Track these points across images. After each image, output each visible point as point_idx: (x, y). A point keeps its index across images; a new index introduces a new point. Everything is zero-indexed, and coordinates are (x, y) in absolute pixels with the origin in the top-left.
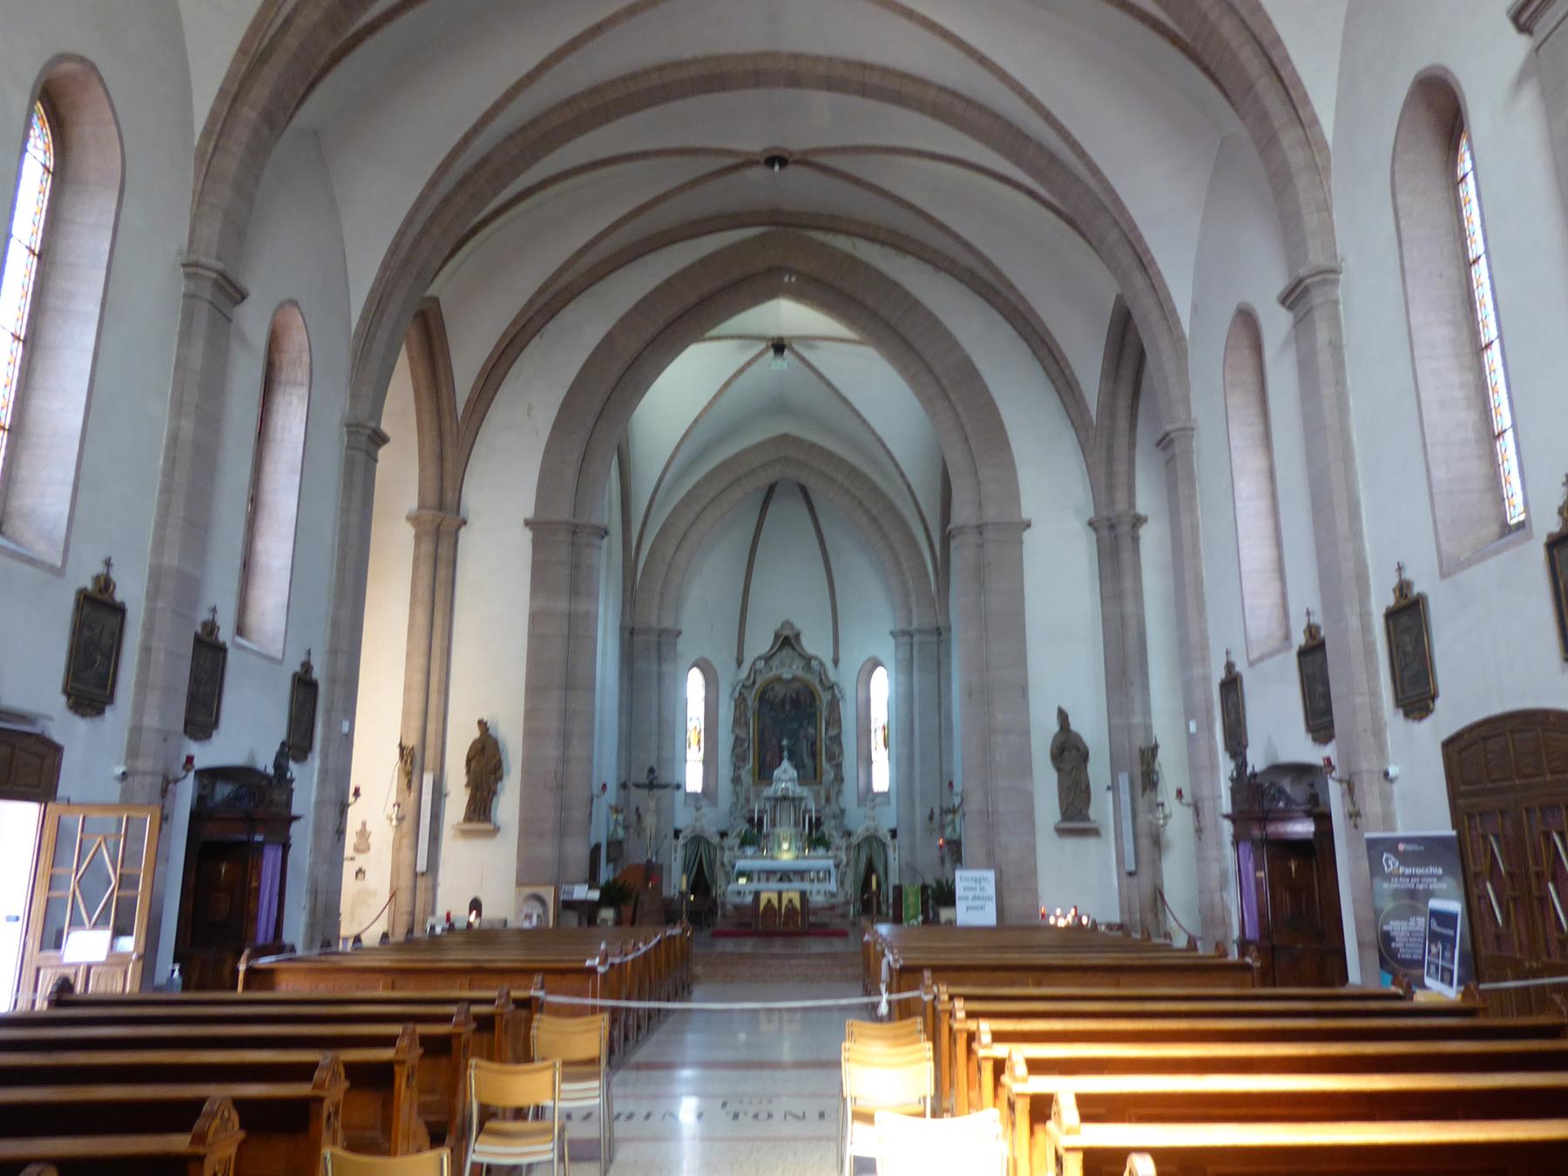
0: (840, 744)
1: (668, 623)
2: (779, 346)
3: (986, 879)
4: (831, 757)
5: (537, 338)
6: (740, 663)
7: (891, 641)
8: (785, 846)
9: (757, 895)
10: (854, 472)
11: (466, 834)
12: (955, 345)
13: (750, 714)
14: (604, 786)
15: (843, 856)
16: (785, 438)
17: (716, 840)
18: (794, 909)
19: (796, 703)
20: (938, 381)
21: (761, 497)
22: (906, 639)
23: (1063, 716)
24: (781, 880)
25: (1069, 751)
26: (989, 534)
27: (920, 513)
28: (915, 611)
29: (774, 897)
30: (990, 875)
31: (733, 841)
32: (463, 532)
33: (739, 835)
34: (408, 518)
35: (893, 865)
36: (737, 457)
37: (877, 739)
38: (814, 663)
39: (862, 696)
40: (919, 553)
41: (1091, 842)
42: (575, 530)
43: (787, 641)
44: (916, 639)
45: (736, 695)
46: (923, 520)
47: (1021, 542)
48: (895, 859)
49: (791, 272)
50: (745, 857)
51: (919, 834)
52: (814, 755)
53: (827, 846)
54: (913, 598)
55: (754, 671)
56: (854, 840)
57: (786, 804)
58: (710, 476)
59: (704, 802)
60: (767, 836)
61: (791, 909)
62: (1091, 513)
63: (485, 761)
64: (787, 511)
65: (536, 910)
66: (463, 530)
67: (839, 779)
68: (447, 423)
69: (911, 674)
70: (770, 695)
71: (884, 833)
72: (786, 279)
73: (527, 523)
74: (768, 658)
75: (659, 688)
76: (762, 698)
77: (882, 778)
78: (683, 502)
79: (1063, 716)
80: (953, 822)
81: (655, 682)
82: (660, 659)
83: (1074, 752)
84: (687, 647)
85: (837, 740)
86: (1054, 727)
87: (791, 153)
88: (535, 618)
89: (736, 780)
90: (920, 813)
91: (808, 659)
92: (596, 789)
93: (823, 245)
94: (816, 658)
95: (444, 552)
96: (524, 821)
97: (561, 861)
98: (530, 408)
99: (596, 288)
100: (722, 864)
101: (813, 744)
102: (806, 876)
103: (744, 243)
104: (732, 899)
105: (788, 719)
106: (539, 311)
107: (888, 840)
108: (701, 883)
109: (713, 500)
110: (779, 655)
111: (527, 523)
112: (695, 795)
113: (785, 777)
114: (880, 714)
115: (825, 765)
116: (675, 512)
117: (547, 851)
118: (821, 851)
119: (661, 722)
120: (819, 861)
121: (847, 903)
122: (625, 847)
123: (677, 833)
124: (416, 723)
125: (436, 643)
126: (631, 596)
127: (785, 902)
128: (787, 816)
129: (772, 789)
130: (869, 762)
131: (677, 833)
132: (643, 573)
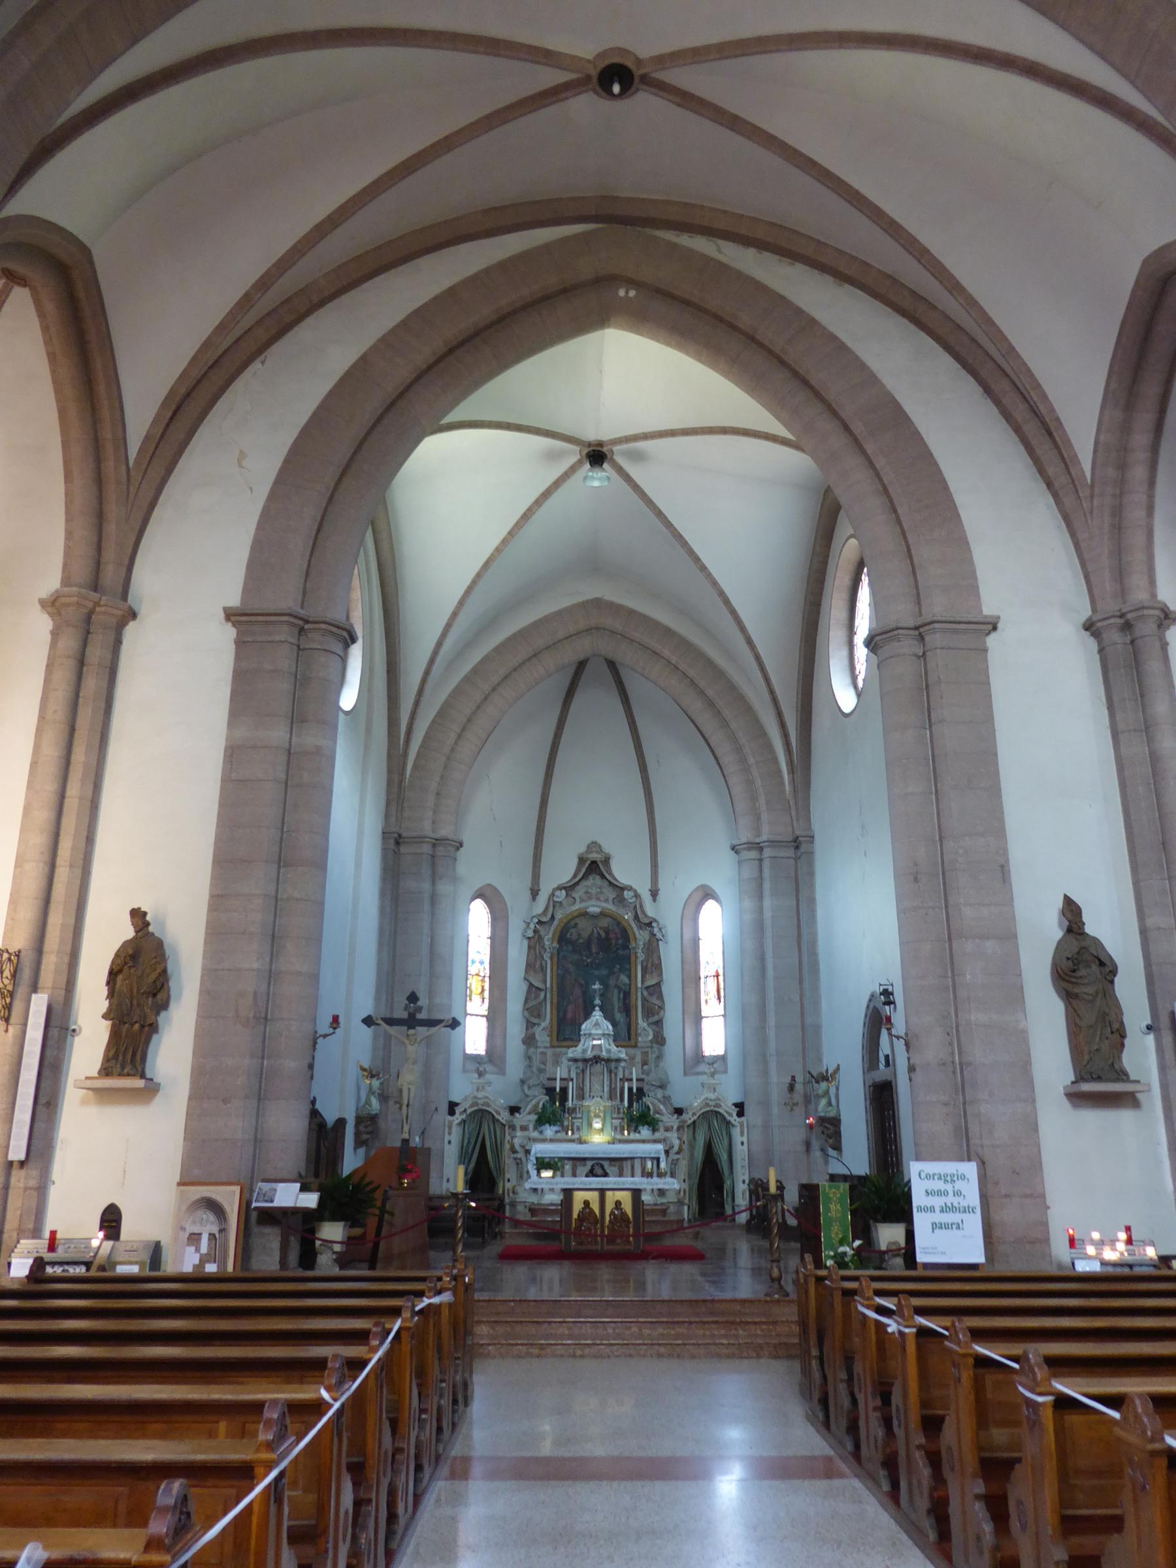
0: (660, 997)
1: (445, 831)
2: (597, 456)
3: (963, 1177)
4: (649, 1012)
5: (256, 365)
6: (535, 893)
7: (729, 858)
8: (597, 1125)
9: (568, 1193)
10: (684, 645)
11: (103, 1096)
12: (871, 379)
13: (547, 956)
14: (336, 1019)
15: (673, 1138)
16: (597, 604)
17: (504, 1117)
18: (624, 1214)
19: (605, 943)
20: (846, 427)
21: (571, 671)
22: (753, 854)
23: (1071, 912)
24: (592, 1173)
25: (1081, 967)
26: (935, 639)
27: (772, 692)
28: (765, 816)
29: (593, 1197)
30: (970, 1169)
31: (526, 1118)
32: (131, 630)
33: (533, 1111)
34: (43, 603)
36: (536, 625)
37: (708, 989)
39: (688, 935)
40: (769, 746)
41: (1124, 1117)
42: (302, 625)
43: (594, 867)
44: (767, 852)
45: (530, 934)
46: (775, 701)
47: (986, 650)
48: (742, 1142)
49: (631, 282)
50: (544, 1141)
51: (775, 1110)
52: (627, 1009)
53: (653, 1124)
54: (762, 801)
55: (552, 903)
56: (688, 1118)
57: (598, 1068)
58: (499, 650)
59: (489, 1067)
60: (573, 1110)
61: (619, 1217)
62: (1086, 612)
63: (141, 979)
64: (596, 701)
65: (207, 1226)
66: (131, 627)
68: (109, 465)
69: (761, 897)
70: (573, 934)
71: (727, 1108)
72: (622, 293)
73: (231, 615)
74: (569, 888)
75: (433, 914)
76: (562, 938)
77: (714, 1039)
78: (467, 679)
79: (1071, 912)
80: (827, 1093)
81: (427, 907)
82: (434, 878)
83: (1095, 967)
84: (472, 866)
85: (656, 990)
86: (1056, 933)
87: (639, 62)
88: (234, 754)
90: (778, 1080)
91: (620, 889)
92: (324, 1026)
93: (674, 247)
94: (630, 888)
95: (97, 653)
96: (200, 1075)
97: (258, 1141)
98: (242, 455)
99: (345, 298)
100: (514, 1151)
101: (627, 995)
102: (627, 1166)
103: (564, 241)
104: (525, 1197)
105: (596, 961)
106: (260, 322)
107: (734, 1119)
108: (483, 1177)
110: (584, 883)
111: (231, 615)
112: (476, 1058)
113: (597, 1034)
114: (712, 955)
115: (642, 1023)
116: (457, 691)
117: (235, 1124)
118: (645, 1132)
119: (433, 955)
120: (644, 1146)
121: (680, 1203)
122: (382, 1123)
123: (452, 1107)
124: (28, 914)
125: (74, 790)
126: (399, 792)
127: (609, 1207)
128: (598, 1083)
129: (580, 1047)
130: (698, 1018)
132: (415, 767)
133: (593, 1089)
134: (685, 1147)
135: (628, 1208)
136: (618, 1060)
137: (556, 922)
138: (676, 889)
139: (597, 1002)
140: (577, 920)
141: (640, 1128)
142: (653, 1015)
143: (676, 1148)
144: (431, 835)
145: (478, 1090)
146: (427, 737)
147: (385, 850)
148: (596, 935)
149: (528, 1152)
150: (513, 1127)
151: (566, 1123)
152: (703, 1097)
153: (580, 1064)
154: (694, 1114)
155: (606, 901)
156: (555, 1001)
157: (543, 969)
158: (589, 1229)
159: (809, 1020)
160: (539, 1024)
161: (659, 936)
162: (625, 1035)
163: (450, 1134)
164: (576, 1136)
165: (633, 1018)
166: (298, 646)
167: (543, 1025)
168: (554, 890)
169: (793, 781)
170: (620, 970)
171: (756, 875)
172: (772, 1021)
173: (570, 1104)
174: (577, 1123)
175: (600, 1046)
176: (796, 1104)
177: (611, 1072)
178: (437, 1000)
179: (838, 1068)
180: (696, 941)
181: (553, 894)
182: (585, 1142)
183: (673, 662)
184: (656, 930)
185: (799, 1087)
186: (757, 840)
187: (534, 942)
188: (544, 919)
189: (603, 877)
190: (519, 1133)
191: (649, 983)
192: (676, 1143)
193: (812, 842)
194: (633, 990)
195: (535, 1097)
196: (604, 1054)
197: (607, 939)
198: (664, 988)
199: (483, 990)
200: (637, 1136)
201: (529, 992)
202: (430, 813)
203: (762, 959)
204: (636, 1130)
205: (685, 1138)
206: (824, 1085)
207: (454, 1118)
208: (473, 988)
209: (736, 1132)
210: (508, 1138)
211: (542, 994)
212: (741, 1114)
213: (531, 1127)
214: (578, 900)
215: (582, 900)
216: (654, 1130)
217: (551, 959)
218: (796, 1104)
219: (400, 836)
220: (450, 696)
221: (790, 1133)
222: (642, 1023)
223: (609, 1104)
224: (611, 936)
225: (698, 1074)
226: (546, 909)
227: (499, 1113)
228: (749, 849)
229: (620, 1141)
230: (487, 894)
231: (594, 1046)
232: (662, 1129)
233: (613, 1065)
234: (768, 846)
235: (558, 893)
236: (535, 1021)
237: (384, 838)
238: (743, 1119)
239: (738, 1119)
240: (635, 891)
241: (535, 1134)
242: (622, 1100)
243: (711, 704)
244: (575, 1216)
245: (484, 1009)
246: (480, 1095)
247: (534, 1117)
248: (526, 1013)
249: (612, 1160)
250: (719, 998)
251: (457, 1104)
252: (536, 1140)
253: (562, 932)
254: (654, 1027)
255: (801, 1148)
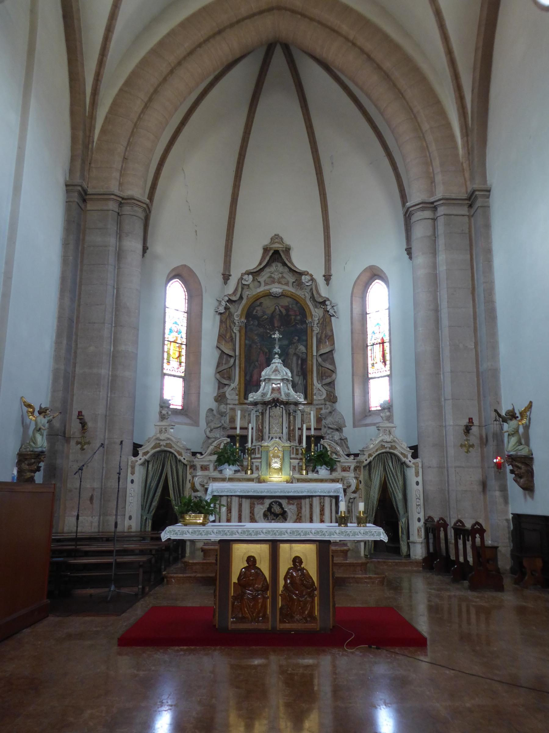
0: (333, 362)
6: (226, 277)
8: (276, 464)
13: (236, 330)
15: (350, 476)
17: (185, 458)
18: (306, 576)
22: (428, 214)
27: (449, 52)
28: (439, 178)
29: (261, 552)
35: (415, 491)
37: (374, 354)
38: (304, 279)
40: (442, 113)
43: (276, 255)
44: (441, 210)
45: (222, 310)
50: (223, 480)
51: (451, 451)
53: (331, 464)
54: (437, 163)
55: (242, 286)
56: (365, 459)
57: (278, 411)
60: (252, 451)
64: (278, 104)
67: (332, 398)
69: (434, 253)
70: (258, 311)
71: (402, 449)
74: (255, 274)
76: (249, 314)
78: (153, 51)
81: (112, 259)
85: (329, 356)
89: (220, 398)
90: (453, 423)
94: (306, 273)
101: (304, 361)
105: (276, 327)
107: (409, 460)
109: (191, 53)
110: (267, 270)
113: (276, 378)
115: (317, 385)
118: (323, 472)
120: (321, 485)
127: (284, 566)
130: (366, 379)
131: (136, 449)
132: (103, 131)
133: (273, 431)
134: (361, 486)
135: (311, 567)
136: (296, 404)
137: (244, 302)
138: (346, 272)
139: (277, 350)
140: (262, 300)
141: (318, 468)
142: (327, 377)
143: (353, 488)
144: (117, 192)
145: (161, 432)
146: (115, 104)
147: (68, 203)
148: (277, 311)
149: (206, 490)
150: (193, 467)
151: (245, 463)
152: (380, 439)
153: (259, 407)
154: (370, 455)
155: (287, 284)
156: (243, 365)
157: (232, 340)
158: (255, 598)
159: (485, 366)
160: (229, 385)
161: (331, 312)
162: (302, 378)
163: (133, 473)
164: (255, 475)
165: (309, 381)
166: (118, 213)
167: (233, 386)
168: (242, 275)
169: (466, 143)
170: (299, 341)
171: (429, 233)
172: (447, 366)
173: (249, 445)
174: (256, 462)
175: (279, 389)
176: (472, 446)
177: (289, 414)
178: (122, 348)
179: (530, 406)
180: (364, 315)
181: (241, 278)
182: (264, 481)
183: (351, 37)
184: (329, 308)
185: (475, 430)
186: (432, 199)
187: (225, 317)
188: (234, 298)
189: (285, 264)
190: (199, 473)
191: (322, 351)
192: (354, 482)
193: (488, 197)
194: (309, 358)
195: (216, 439)
196: (283, 398)
197: (288, 315)
198: (336, 356)
199: (180, 356)
200: (315, 476)
201: (220, 358)
202: (117, 175)
203: (436, 310)
204: (314, 470)
205: (361, 478)
206: (513, 423)
207: (137, 458)
208: (171, 352)
209: (410, 473)
210: (189, 477)
211: (232, 360)
212: (415, 456)
213: (211, 467)
214: (263, 284)
215: (266, 284)
216: (332, 470)
217: (240, 331)
218: (472, 446)
219: (85, 191)
220: (137, 66)
221: (465, 475)
222: (317, 385)
223: (287, 444)
224: (291, 313)
225: (366, 425)
226: (236, 290)
227: (181, 454)
228: (423, 209)
229: (299, 480)
230: (182, 274)
231: (273, 389)
232: (339, 469)
233: (292, 407)
234: (443, 204)
235: (246, 277)
236: (226, 382)
237: (67, 191)
238: (417, 460)
239: (413, 461)
240: (311, 276)
241: (216, 474)
242: (300, 442)
243: (387, 76)
244: (234, 579)
245: (181, 371)
246: (163, 437)
247: (215, 457)
248: (218, 376)
249: (290, 498)
250: (384, 362)
251: (141, 446)
252: (215, 480)
253: (249, 309)
254: (327, 388)
255: (477, 488)
